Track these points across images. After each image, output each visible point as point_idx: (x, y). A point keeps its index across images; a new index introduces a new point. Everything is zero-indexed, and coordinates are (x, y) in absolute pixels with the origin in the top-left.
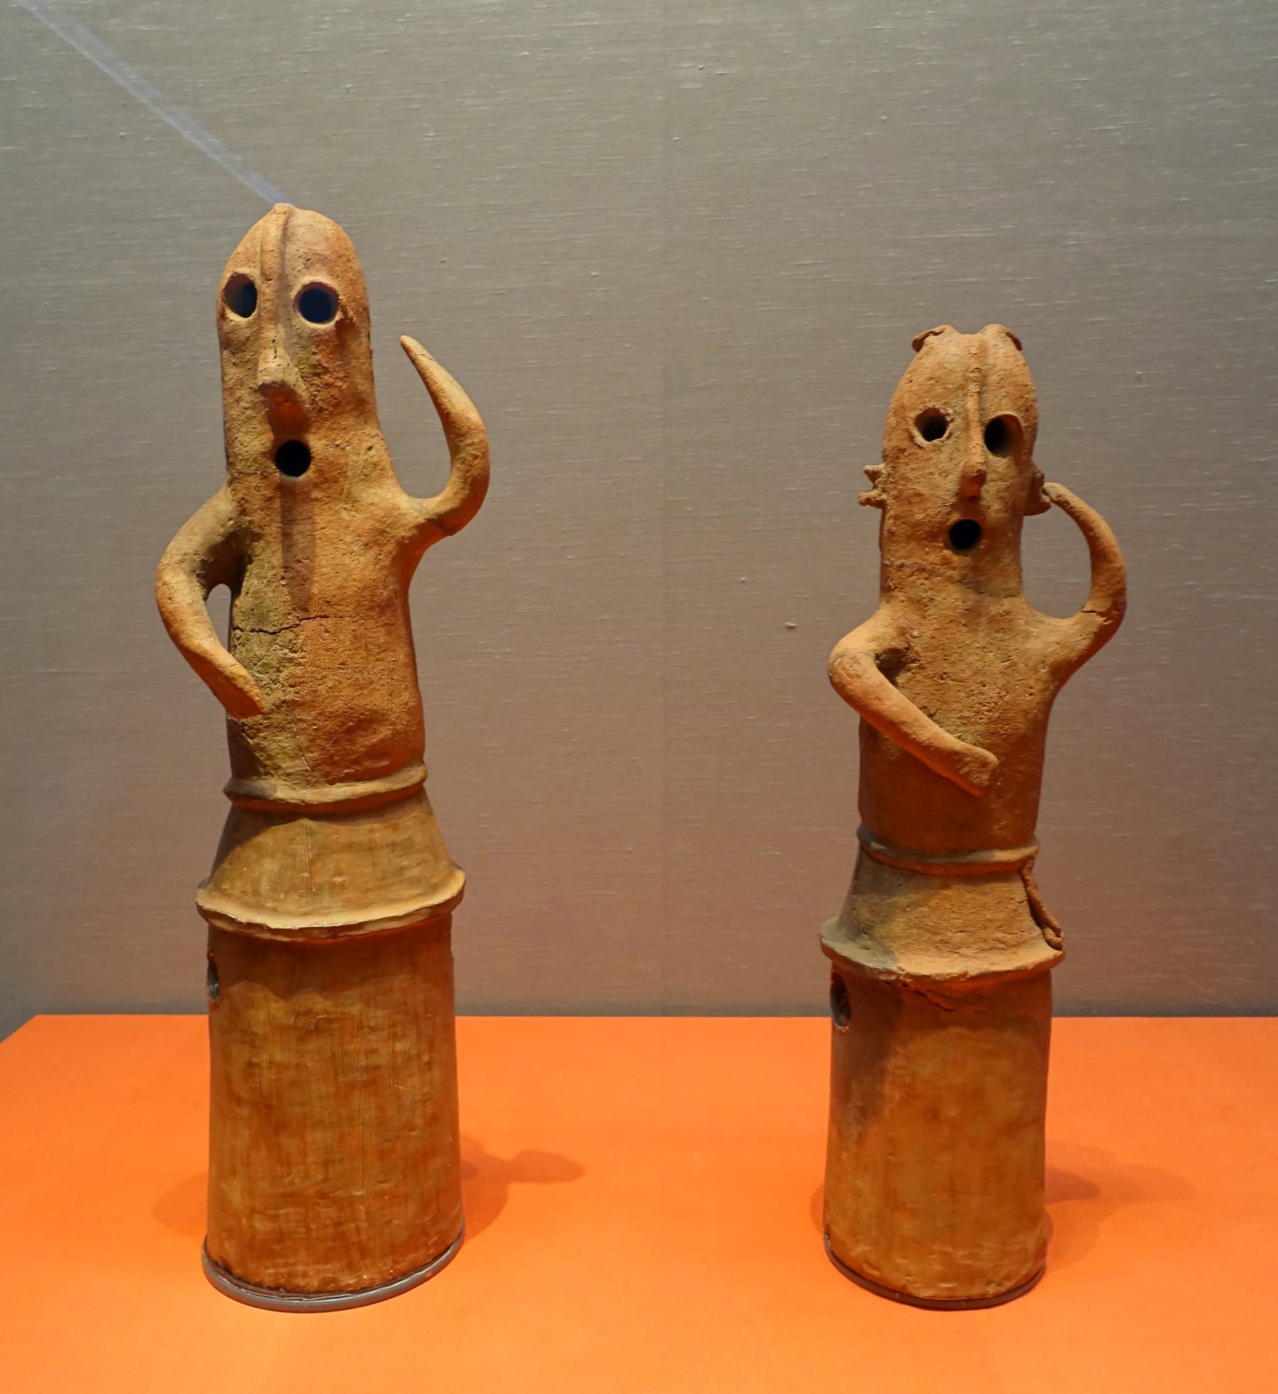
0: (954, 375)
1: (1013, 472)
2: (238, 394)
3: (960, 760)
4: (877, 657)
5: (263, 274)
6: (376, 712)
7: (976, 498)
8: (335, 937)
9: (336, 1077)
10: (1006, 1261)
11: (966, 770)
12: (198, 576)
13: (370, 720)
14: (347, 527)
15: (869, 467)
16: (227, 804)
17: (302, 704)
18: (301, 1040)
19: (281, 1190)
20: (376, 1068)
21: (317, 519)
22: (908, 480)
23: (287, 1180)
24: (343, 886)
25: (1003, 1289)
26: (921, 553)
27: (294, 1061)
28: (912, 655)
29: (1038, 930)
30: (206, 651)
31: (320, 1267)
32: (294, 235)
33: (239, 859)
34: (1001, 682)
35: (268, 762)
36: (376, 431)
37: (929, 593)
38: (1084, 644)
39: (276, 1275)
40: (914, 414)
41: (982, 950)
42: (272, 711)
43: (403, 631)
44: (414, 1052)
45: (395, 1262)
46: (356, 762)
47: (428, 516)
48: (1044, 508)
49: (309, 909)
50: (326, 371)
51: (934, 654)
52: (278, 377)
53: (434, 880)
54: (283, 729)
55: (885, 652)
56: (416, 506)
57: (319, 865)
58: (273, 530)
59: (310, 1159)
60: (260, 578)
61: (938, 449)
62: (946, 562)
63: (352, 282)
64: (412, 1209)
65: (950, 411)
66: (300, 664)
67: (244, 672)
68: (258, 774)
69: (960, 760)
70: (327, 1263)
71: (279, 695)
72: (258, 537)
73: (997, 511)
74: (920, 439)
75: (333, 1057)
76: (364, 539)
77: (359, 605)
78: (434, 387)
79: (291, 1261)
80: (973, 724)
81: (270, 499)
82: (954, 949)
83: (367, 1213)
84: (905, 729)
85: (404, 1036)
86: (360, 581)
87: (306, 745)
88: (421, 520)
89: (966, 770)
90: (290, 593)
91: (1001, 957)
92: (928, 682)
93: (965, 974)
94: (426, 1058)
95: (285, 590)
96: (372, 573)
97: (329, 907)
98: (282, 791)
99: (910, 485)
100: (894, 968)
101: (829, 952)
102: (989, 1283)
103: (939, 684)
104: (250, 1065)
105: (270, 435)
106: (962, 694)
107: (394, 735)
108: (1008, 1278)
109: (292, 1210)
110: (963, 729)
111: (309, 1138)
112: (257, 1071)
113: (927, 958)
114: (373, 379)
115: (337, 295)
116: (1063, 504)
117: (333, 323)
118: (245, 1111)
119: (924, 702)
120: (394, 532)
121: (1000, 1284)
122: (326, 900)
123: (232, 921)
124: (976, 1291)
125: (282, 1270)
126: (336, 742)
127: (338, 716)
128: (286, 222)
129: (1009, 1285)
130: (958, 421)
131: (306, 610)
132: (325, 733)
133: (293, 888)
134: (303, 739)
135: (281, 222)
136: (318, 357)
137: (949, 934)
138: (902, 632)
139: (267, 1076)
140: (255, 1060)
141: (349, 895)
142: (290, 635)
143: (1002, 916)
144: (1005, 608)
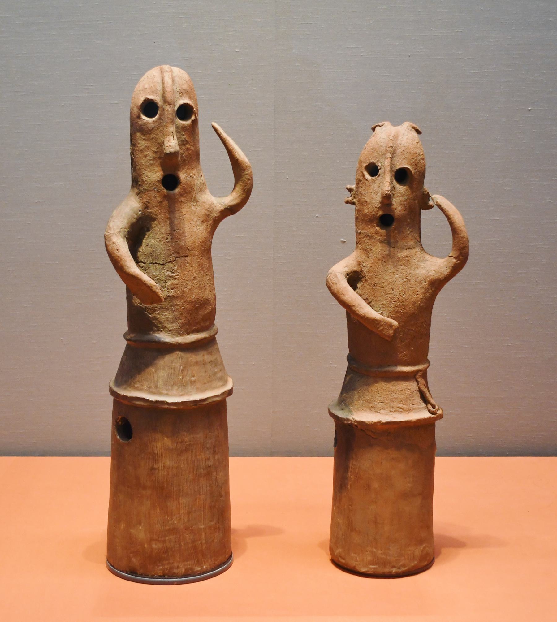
1: (409, 192)
2: (146, 153)
3: (378, 324)
4: (348, 274)
7: (390, 204)
8: (196, 405)
9: (193, 472)
10: (403, 558)
11: (382, 328)
15: (348, 186)
17: (177, 297)
19: (167, 528)
20: (209, 467)
22: (362, 194)
23: (170, 522)
24: (195, 382)
26: (367, 228)
29: (424, 405)
31: (185, 563)
32: (163, 79)
35: (160, 325)
37: (370, 247)
38: (447, 271)
39: (163, 570)
40: (365, 165)
45: (216, 560)
46: (197, 323)
49: (183, 393)
54: (168, 309)
55: (351, 272)
59: (182, 512)
60: (154, 238)
61: (374, 181)
62: (377, 233)
65: (380, 164)
66: (176, 279)
69: (378, 324)
71: (166, 293)
72: (155, 219)
73: (400, 211)
74: (367, 176)
75: (193, 462)
80: (387, 307)
81: (161, 202)
82: (378, 411)
83: (205, 536)
88: (222, 208)
89: (382, 328)
92: (369, 287)
93: (380, 422)
97: (191, 392)
98: (165, 337)
99: (363, 197)
100: (350, 418)
101: (332, 415)
103: (373, 288)
104: (153, 469)
108: (404, 566)
109: (172, 537)
111: (181, 502)
112: (157, 471)
116: (439, 206)
118: (149, 492)
119: (366, 296)
121: (399, 568)
122: (189, 388)
123: (217, 396)
124: (387, 570)
125: (166, 567)
126: (191, 314)
129: (403, 569)
131: (178, 253)
133: (175, 384)
136: (185, 137)
137: (376, 403)
138: (359, 263)
140: (156, 466)
141: (198, 385)
142: (171, 265)
144: (406, 254)
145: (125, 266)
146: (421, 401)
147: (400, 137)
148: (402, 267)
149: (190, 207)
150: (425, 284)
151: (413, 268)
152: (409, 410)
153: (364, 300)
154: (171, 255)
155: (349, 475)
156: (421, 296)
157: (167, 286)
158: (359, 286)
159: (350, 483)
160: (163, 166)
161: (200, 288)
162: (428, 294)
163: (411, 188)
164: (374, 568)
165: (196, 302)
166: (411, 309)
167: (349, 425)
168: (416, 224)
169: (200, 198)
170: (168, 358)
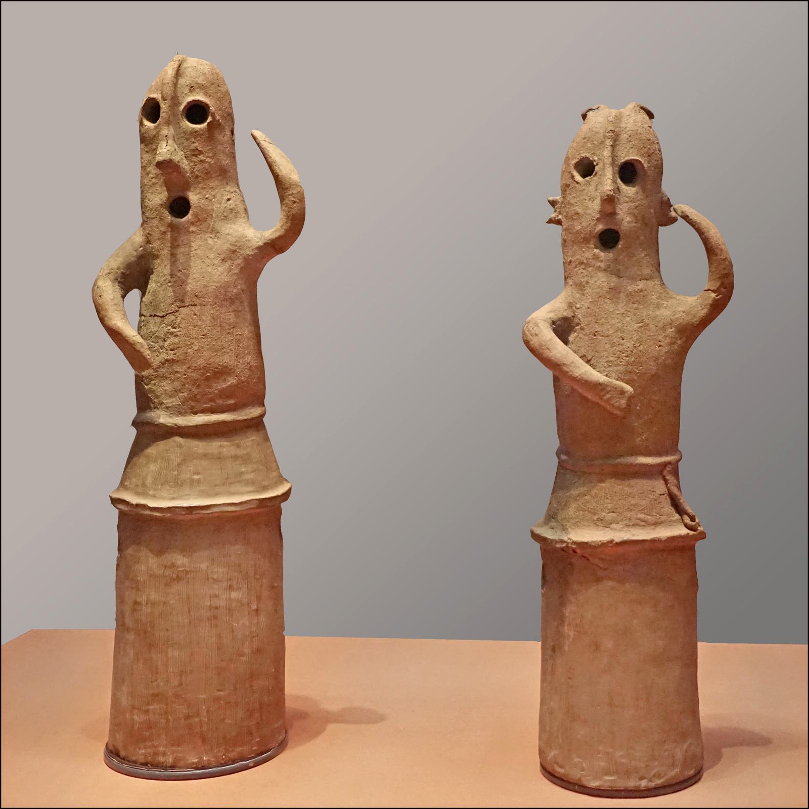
0: (598, 135)
3: (603, 389)
4: (554, 323)
5: (163, 97)
6: (226, 367)
7: (613, 214)
10: (656, 763)
12: (119, 282)
13: (222, 372)
14: (211, 249)
15: (551, 199)
16: (134, 432)
17: (178, 361)
18: (166, 585)
19: (151, 692)
20: (216, 608)
21: (193, 244)
22: (572, 204)
23: (155, 684)
24: (199, 481)
25: (652, 784)
27: (163, 599)
28: (576, 321)
29: (677, 516)
30: (119, 328)
33: (135, 465)
34: (635, 337)
36: (235, 189)
37: (586, 279)
38: (703, 312)
40: (573, 162)
41: (628, 526)
42: (159, 367)
43: (249, 316)
44: (245, 600)
47: (265, 241)
48: (673, 220)
49: (175, 495)
50: (201, 152)
51: (589, 319)
52: (167, 157)
53: (265, 483)
56: (259, 235)
57: (184, 467)
58: (165, 252)
61: (589, 183)
63: (220, 99)
64: (240, 713)
65: (596, 158)
67: (141, 340)
68: (150, 408)
70: (179, 745)
71: (163, 356)
72: (156, 257)
74: (578, 177)
75: (188, 598)
76: (222, 256)
77: (216, 296)
78: (270, 160)
79: (156, 744)
80: (616, 365)
82: (607, 525)
83: (208, 711)
84: (565, 368)
85: (239, 589)
86: (218, 282)
87: (179, 388)
88: (261, 244)
90: (174, 291)
91: (641, 531)
92: (586, 337)
93: (612, 541)
94: (254, 607)
95: (171, 289)
96: (225, 278)
98: (164, 418)
100: (565, 538)
101: (536, 537)
102: (641, 779)
103: (593, 339)
104: (136, 603)
105: (166, 194)
106: (607, 346)
107: (238, 383)
108: (658, 776)
110: (609, 369)
111: (170, 655)
113: (588, 532)
114: (234, 157)
115: (209, 107)
116: (686, 217)
117: (206, 124)
119: (583, 351)
120: (242, 252)
122: (187, 490)
124: (632, 783)
125: (149, 750)
126: (199, 386)
127: (200, 369)
128: (180, 66)
129: (659, 782)
130: (601, 165)
132: (191, 380)
133: (165, 482)
134: (177, 384)
135: (176, 66)
136: (196, 144)
137: (604, 514)
138: (570, 305)
139: (146, 610)
140: (138, 600)
141: (202, 488)
142: (172, 317)
143: (644, 502)
144: (640, 287)
145: (106, 316)
146: (673, 510)
147: (624, 120)
148: (636, 305)
149: (206, 240)
150: (671, 331)
151: (651, 307)
152: (656, 524)
153: (581, 357)
154: (173, 304)
155: (566, 629)
156: (666, 349)
157: (165, 345)
158: (571, 338)
159: (567, 643)
160: (168, 185)
161: (213, 349)
162: (676, 347)
163: (644, 190)
164: (612, 780)
165: (206, 368)
166: (652, 368)
167: (563, 549)
168: (653, 245)
169: (223, 229)
170: (162, 445)
